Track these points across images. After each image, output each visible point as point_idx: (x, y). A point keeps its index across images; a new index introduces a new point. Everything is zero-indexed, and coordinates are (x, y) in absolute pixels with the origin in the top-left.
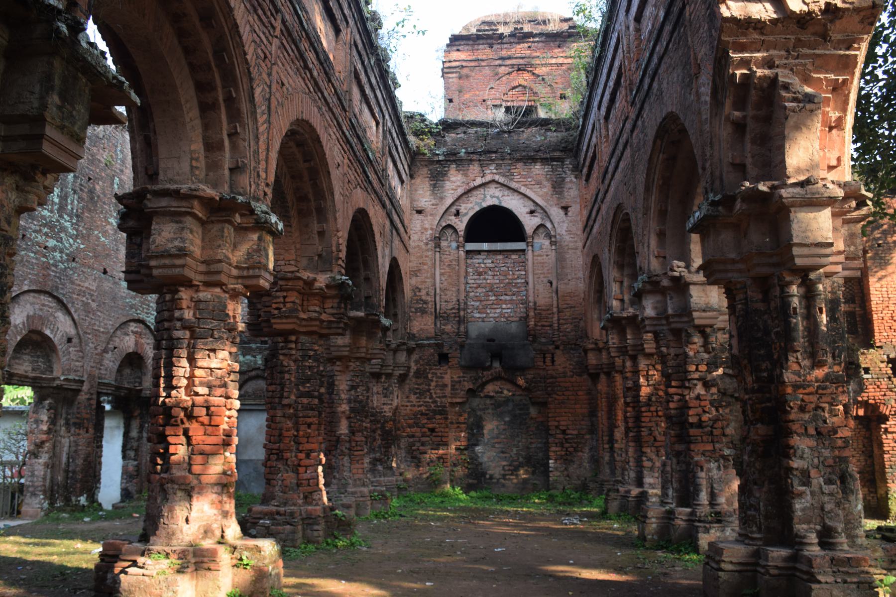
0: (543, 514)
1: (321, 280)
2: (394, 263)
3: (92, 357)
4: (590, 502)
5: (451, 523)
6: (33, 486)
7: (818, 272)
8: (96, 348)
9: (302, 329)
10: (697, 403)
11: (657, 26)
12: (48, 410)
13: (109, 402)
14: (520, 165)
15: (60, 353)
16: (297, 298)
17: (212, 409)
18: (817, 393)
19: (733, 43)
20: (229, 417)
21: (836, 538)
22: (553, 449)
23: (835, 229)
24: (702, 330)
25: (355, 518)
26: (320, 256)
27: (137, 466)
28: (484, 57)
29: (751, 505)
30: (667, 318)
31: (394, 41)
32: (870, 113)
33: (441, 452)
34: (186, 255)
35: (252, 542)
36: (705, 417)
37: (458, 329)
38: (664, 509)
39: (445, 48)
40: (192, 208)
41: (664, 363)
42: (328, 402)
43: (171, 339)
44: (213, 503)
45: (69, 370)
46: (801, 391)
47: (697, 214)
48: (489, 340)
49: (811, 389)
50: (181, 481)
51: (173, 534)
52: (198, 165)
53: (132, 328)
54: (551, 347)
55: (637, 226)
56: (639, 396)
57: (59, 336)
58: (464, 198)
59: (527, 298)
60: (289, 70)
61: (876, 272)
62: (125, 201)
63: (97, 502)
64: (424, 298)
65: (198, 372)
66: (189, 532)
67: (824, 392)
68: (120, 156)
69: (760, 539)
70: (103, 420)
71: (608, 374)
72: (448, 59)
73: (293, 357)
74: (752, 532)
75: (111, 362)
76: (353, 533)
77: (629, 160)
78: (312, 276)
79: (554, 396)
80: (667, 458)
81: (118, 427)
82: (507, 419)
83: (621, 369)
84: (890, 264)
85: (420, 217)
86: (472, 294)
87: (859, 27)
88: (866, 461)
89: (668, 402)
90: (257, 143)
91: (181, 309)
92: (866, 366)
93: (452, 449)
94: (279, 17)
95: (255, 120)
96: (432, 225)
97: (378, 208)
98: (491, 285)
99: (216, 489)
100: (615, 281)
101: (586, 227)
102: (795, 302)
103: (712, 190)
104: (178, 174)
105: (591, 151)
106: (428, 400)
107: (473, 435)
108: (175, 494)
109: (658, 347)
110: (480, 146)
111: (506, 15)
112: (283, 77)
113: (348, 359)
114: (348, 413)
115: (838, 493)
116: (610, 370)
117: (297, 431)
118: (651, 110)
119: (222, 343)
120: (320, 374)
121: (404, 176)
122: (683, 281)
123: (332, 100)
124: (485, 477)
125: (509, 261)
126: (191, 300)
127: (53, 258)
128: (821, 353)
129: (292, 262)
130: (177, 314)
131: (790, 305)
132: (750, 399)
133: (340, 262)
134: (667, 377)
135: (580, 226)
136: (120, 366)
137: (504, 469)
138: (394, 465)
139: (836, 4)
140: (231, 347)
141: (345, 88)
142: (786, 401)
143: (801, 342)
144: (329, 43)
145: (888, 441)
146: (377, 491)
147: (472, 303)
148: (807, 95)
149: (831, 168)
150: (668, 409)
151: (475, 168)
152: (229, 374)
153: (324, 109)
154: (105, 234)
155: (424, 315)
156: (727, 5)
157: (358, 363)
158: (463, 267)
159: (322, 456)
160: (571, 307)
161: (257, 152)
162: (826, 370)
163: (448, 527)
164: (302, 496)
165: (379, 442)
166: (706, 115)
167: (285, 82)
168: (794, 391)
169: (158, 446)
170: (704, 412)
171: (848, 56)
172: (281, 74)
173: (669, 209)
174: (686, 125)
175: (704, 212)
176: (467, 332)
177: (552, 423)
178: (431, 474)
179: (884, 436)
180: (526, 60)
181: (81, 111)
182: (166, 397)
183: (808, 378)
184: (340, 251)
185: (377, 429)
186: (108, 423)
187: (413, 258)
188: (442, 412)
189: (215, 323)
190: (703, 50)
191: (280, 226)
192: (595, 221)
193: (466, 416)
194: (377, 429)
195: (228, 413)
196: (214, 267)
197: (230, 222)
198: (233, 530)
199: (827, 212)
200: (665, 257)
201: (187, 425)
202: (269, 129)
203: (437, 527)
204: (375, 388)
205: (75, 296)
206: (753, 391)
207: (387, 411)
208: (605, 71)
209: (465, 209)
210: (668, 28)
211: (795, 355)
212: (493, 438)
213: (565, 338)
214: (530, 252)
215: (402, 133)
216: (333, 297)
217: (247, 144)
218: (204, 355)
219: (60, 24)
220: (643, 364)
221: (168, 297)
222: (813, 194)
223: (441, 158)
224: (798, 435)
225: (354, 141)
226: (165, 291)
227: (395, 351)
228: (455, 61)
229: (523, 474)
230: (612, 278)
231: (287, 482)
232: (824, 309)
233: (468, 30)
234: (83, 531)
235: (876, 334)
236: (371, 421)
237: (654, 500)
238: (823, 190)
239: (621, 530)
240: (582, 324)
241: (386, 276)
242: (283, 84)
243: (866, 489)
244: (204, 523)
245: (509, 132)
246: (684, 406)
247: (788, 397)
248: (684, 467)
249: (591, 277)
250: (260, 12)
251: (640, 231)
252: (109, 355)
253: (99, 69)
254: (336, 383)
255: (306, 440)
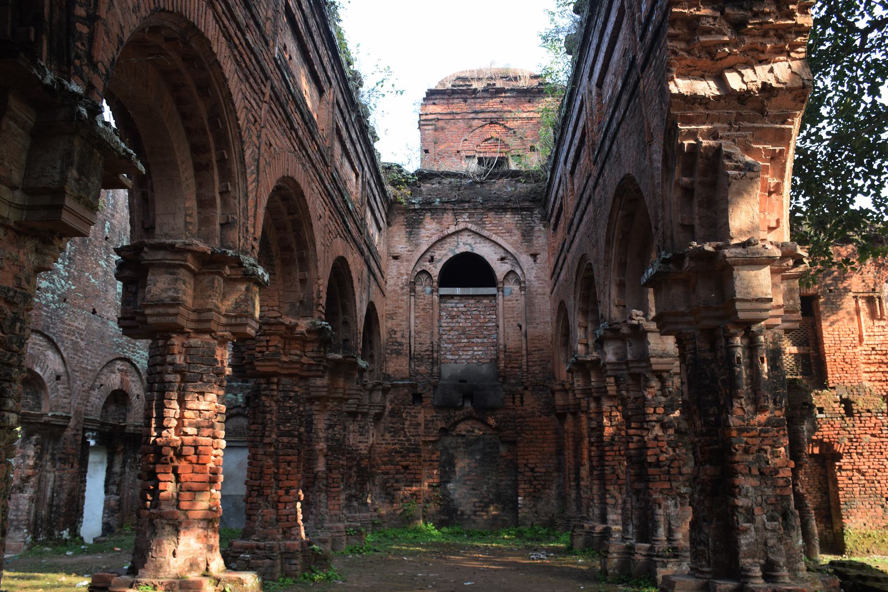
0: (511, 550)
1: (302, 325)
2: (371, 308)
4: (557, 537)
5: (423, 558)
7: (759, 325)
9: (283, 372)
10: (654, 443)
11: (616, 94)
12: (35, 445)
13: (93, 438)
14: (491, 214)
15: (49, 390)
17: (200, 448)
18: (759, 436)
20: (216, 456)
21: (776, 571)
23: (774, 285)
24: (659, 375)
25: (331, 553)
26: (301, 302)
27: (119, 501)
28: (459, 111)
29: (701, 541)
30: (627, 363)
31: (373, 99)
33: (414, 488)
34: (179, 304)
35: (234, 575)
36: (663, 457)
37: (432, 370)
38: (624, 545)
40: (186, 261)
42: (306, 441)
43: (162, 382)
44: (198, 538)
45: (57, 407)
46: (745, 434)
47: (650, 270)
48: (461, 381)
49: (754, 433)
50: (170, 516)
51: (161, 567)
53: (118, 366)
54: (520, 388)
56: (602, 436)
57: (48, 373)
58: (438, 245)
59: (498, 340)
60: (277, 131)
61: (828, 316)
62: (123, 253)
63: (79, 535)
64: (399, 340)
65: (187, 414)
66: (176, 565)
67: (766, 435)
69: (710, 572)
70: (87, 455)
71: (574, 414)
72: (424, 112)
73: (275, 398)
74: (702, 566)
75: (97, 399)
76: (329, 567)
77: (592, 214)
78: (294, 321)
79: (523, 435)
80: (627, 496)
81: (101, 462)
82: (478, 457)
83: (586, 409)
84: (841, 309)
85: (396, 262)
86: (445, 337)
87: (793, 104)
88: (822, 497)
89: (628, 442)
90: (247, 201)
91: (173, 354)
94: (269, 84)
95: (245, 179)
96: (407, 270)
97: (357, 255)
98: (464, 328)
99: (202, 524)
100: (580, 326)
101: (553, 273)
102: (739, 352)
103: (664, 248)
107: (446, 472)
108: (163, 528)
109: (618, 391)
110: (454, 196)
111: (480, 71)
112: (270, 138)
113: (327, 399)
114: (325, 451)
115: (780, 529)
116: (576, 411)
117: (278, 468)
118: (611, 170)
121: (382, 224)
122: (641, 329)
123: (315, 157)
124: (456, 513)
126: (183, 346)
127: (46, 299)
128: (762, 399)
130: (169, 359)
131: (734, 356)
132: (699, 441)
133: (320, 308)
134: (627, 418)
135: (548, 272)
136: (105, 403)
137: (474, 506)
138: (369, 501)
139: (771, 84)
140: (219, 390)
141: (327, 144)
142: (732, 444)
143: (744, 388)
144: (313, 103)
146: (353, 527)
148: (747, 164)
149: (771, 229)
150: (627, 449)
151: (448, 217)
152: (216, 415)
154: (95, 275)
155: (399, 357)
156: (675, 83)
157: (335, 403)
158: (437, 311)
159: (301, 493)
160: (539, 350)
161: (246, 209)
162: (768, 415)
164: (281, 531)
166: (658, 180)
167: (273, 142)
168: (739, 434)
169: (149, 483)
170: (662, 452)
171: (783, 129)
172: (270, 136)
173: (628, 261)
174: (641, 187)
175: (656, 268)
176: (440, 373)
177: (521, 461)
178: (405, 510)
179: (838, 474)
180: (498, 114)
181: (95, 180)
182: (157, 437)
183: (752, 422)
184: (321, 298)
185: (352, 466)
186: (92, 458)
187: (389, 302)
188: (416, 450)
189: (205, 367)
191: (266, 278)
192: (561, 269)
193: (439, 454)
194: (352, 466)
195: (214, 452)
197: (220, 274)
198: (217, 564)
199: (767, 270)
201: (176, 464)
202: (257, 187)
203: (409, 561)
204: (351, 427)
205: (65, 335)
207: (363, 449)
208: (571, 129)
210: (625, 97)
211: (739, 401)
212: (464, 475)
213: (533, 379)
214: (501, 297)
215: (380, 183)
216: (313, 341)
218: (193, 397)
219: (81, 108)
220: (606, 405)
221: (161, 343)
222: (754, 254)
223: (417, 207)
224: (743, 475)
225: (335, 194)
226: (158, 337)
227: (371, 391)
228: (431, 114)
229: (493, 511)
230: (577, 323)
231: (267, 518)
232: (765, 359)
233: (444, 85)
234: (66, 565)
235: (829, 375)
236: (347, 459)
237: (617, 535)
239: (585, 565)
240: (550, 366)
241: (363, 320)
242: (271, 145)
243: (823, 525)
244: (190, 556)
245: (481, 183)
246: (643, 447)
247: (734, 440)
248: (643, 505)
249: (558, 322)
250: (252, 80)
251: (601, 281)
253: (112, 145)
254: (315, 422)
255: (285, 477)
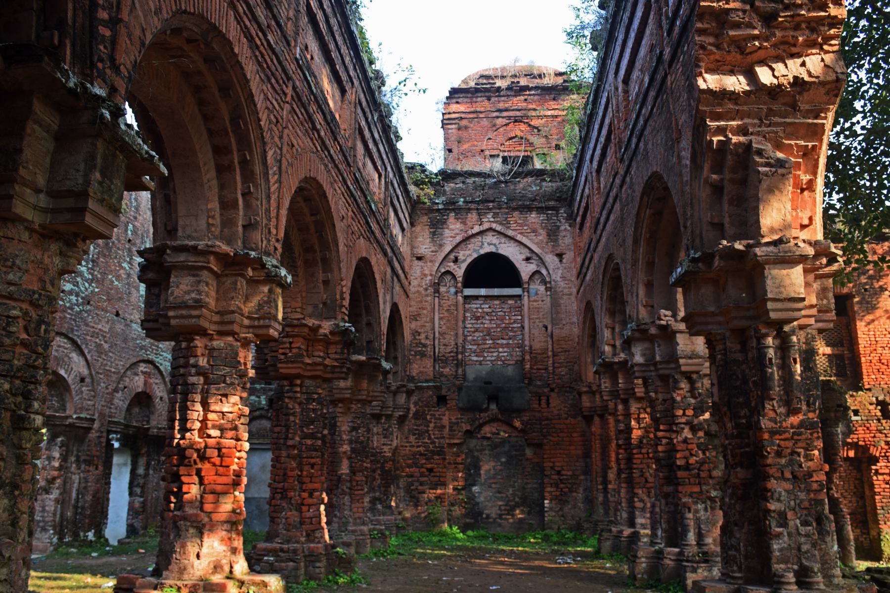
0: (537, 554)
2: (395, 309)
3: (103, 397)
5: (448, 562)
6: (43, 521)
7: (792, 325)
8: (107, 388)
9: (307, 374)
10: (683, 446)
11: (643, 90)
12: (60, 447)
13: (117, 440)
14: (516, 214)
16: (302, 344)
17: (224, 450)
18: (792, 438)
19: (710, 112)
20: (239, 458)
21: (813, 577)
22: (549, 489)
23: (807, 285)
24: (688, 376)
25: (355, 556)
26: (325, 304)
28: (482, 109)
29: (732, 545)
30: (655, 364)
31: (396, 99)
32: (851, 165)
33: (439, 491)
34: (202, 306)
35: (258, 578)
36: (693, 460)
37: (456, 371)
38: (653, 549)
39: (445, 100)
40: (208, 263)
41: (653, 407)
42: (330, 444)
43: (186, 384)
44: (222, 540)
45: (82, 409)
46: (777, 437)
47: (679, 270)
48: (486, 383)
50: (193, 518)
51: (185, 569)
52: (214, 222)
53: (141, 369)
54: (546, 390)
55: (626, 276)
56: (630, 438)
57: (72, 376)
58: (462, 245)
61: (864, 316)
62: (146, 255)
63: (104, 537)
64: (423, 341)
65: (211, 416)
66: (200, 568)
67: (799, 438)
68: (134, 204)
69: (741, 578)
70: (111, 457)
71: (602, 417)
72: (447, 111)
73: (298, 400)
74: (733, 572)
75: (121, 401)
77: (619, 213)
78: (316, 322)
84: (877, 308)
85: (420, 263)
86: (469, 338)
87: (825, 98)
88: (858, 502)
89: (657, 445)
90: (269, 202)
91: (196, 356)
92: (855, 408)
93: (450, 489)
95: (267, 180)
96: (431, 271)
97: (380, 256)
99: (225, 526)
100: (607, 327)
102: (771, 353)
104: (196, 231)
105: (584, 201)
106: (426, 440)
107: (470, 475)
108: (187, 531)
109: (647, 392)
110: (478, 195)
115: (814, 534)
116: (603, 413)
117: (301, 471)
118: (638, 168)
119: (233, 389)
120: (323, 416)
121: (405, 225)
123: (338, 157)
125: (506, 306)
127: (70, 301)
128: (795, 401)
129: (298, 310)
132: (730, 444)
133: (344, 310)
134: (656, 421)
136: (129, 405)
137: (500, 509)
138: (393, 504)
139: (803, 78)
142: (763, 446)
143: (776, 389)
144: (335, 103)
145: (879, 483)
146: (377, 530)
147: (470, 347)
148: (778, 160)
149: (803, 227)
151: (473, 216)
152: (240, 418)
153: (330, 166)
154: (118, 277)
156: (703, 78)
158: (461, 312)
159: (324, 495)
161: (268, 211)
162: (801, 417)
163: (446, 566)
164: (304, 534)
165: (379, 481)
167: (295, 143)
168: (771, 437)
169: (172, 485)
170: (692, 455)
171: (816, 124)
172: (292, 137)
173: (656, 260)
174: (669, 185)
176: (464, 375)
177: (547, 464)
178: (429, 514)
179: (875, 478)
181: (118, 182)
183: (784, 424)
184: (344, 299)
185: (376, 469)
186: (116, 460)
187: (413, 303)
188: (441, 452)
189: (228, 369)
190: (683, 117)
191: (289, 279)
192: (588, 269)
193: (464, 456)
194: (376, 469)
195: (238, 454)
196: (228, 318)
197: (243, 276)
198: (241, 566)
199: (799, 269)
200: (652, 307)
201: (200, 466)
203: (434, 565)
205: (89, 338)
206: (733, 437)
207: (387, 452)
208: (596, 127)
209: (464, 255)
210: (652, 94)
212: (489, 478)
214: (526, 298)
215: (403, 184)
216: (336, 343)
217: (259, 203)
219: (104, 111)
220: (634, 407)
221: (184, 345)
222: (786, 252)
223: (440, 207)
224: (775, 479)
225: (358, 194)
226: (181, 339)
227: (395, 393)
228: (454, 113)
231: (291, 520)
232: (798, 360)
233: (467, 83)
234: (91, 566)
236: (371, 461)
237: (645, 540)
238: (795, 248)
240: (576, 367)
241: (387, 321)
242: (293, 146)
243: (858, 531)
244: (214, 559)
245: (506, 182)
246: (672, 449)
247: (766, 443)
249: (584, 322)
250: (273, 81)
251: (629, 281)
252: (119, 395)
254: (338, 424)
